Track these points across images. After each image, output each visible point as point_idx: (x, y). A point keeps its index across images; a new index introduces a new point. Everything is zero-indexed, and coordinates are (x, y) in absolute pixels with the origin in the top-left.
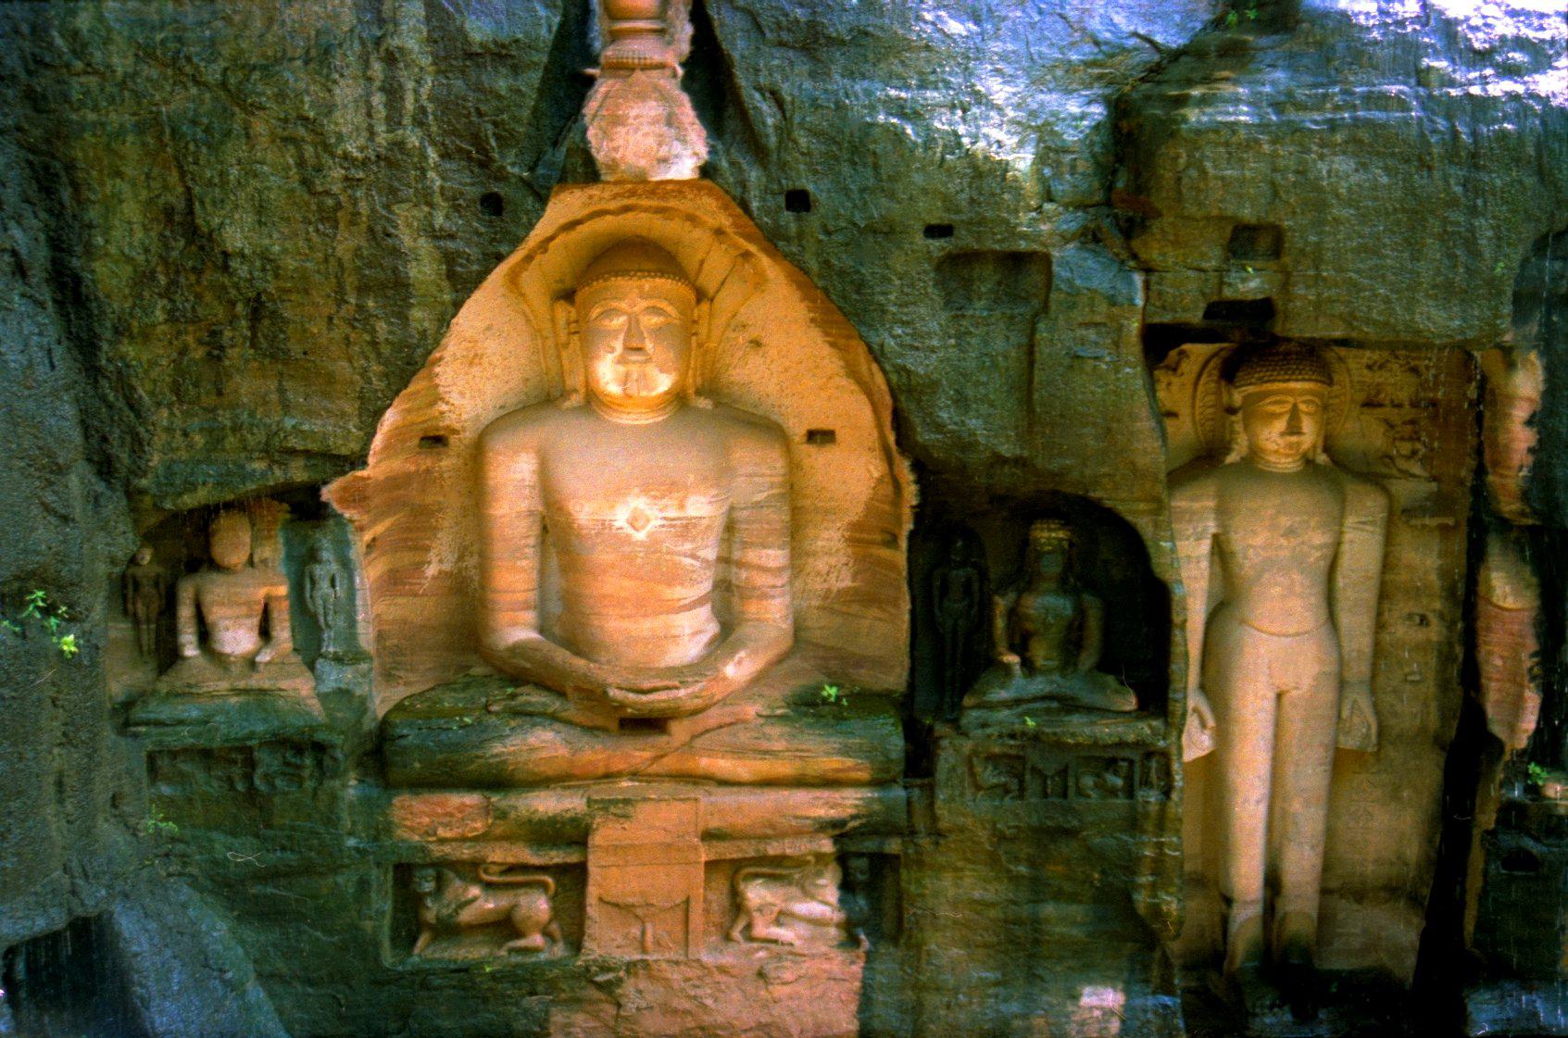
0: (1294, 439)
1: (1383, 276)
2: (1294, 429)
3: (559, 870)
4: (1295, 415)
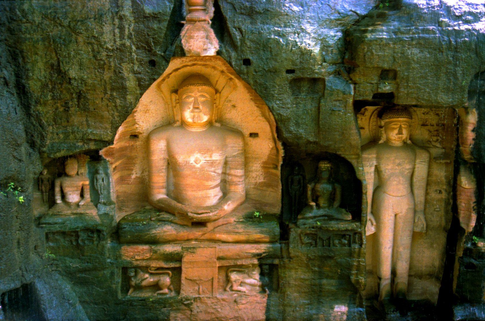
0: (400, 136)
1: (428, 85)
2: (400, 133)
3: (173, 269)
4: (400, 128)
